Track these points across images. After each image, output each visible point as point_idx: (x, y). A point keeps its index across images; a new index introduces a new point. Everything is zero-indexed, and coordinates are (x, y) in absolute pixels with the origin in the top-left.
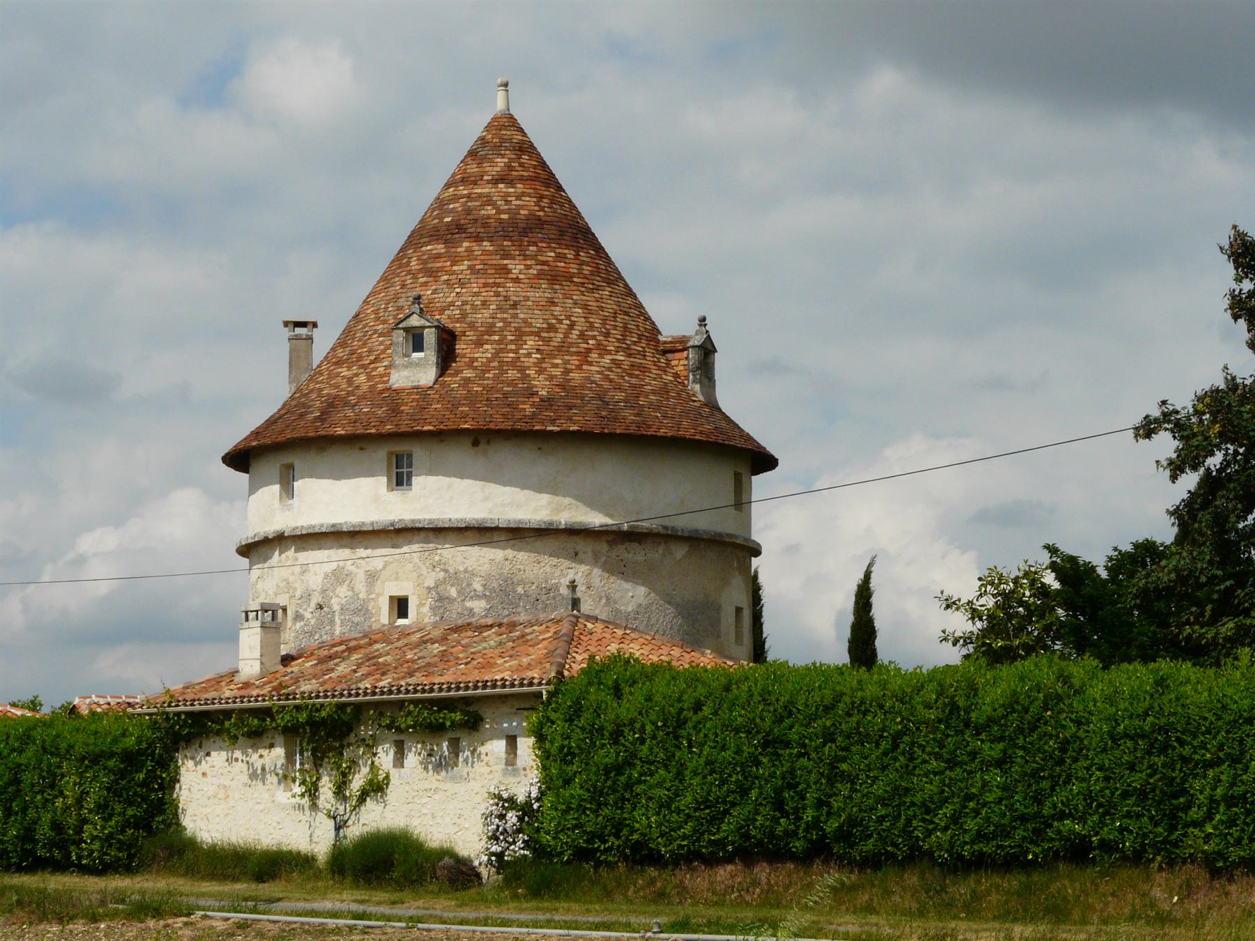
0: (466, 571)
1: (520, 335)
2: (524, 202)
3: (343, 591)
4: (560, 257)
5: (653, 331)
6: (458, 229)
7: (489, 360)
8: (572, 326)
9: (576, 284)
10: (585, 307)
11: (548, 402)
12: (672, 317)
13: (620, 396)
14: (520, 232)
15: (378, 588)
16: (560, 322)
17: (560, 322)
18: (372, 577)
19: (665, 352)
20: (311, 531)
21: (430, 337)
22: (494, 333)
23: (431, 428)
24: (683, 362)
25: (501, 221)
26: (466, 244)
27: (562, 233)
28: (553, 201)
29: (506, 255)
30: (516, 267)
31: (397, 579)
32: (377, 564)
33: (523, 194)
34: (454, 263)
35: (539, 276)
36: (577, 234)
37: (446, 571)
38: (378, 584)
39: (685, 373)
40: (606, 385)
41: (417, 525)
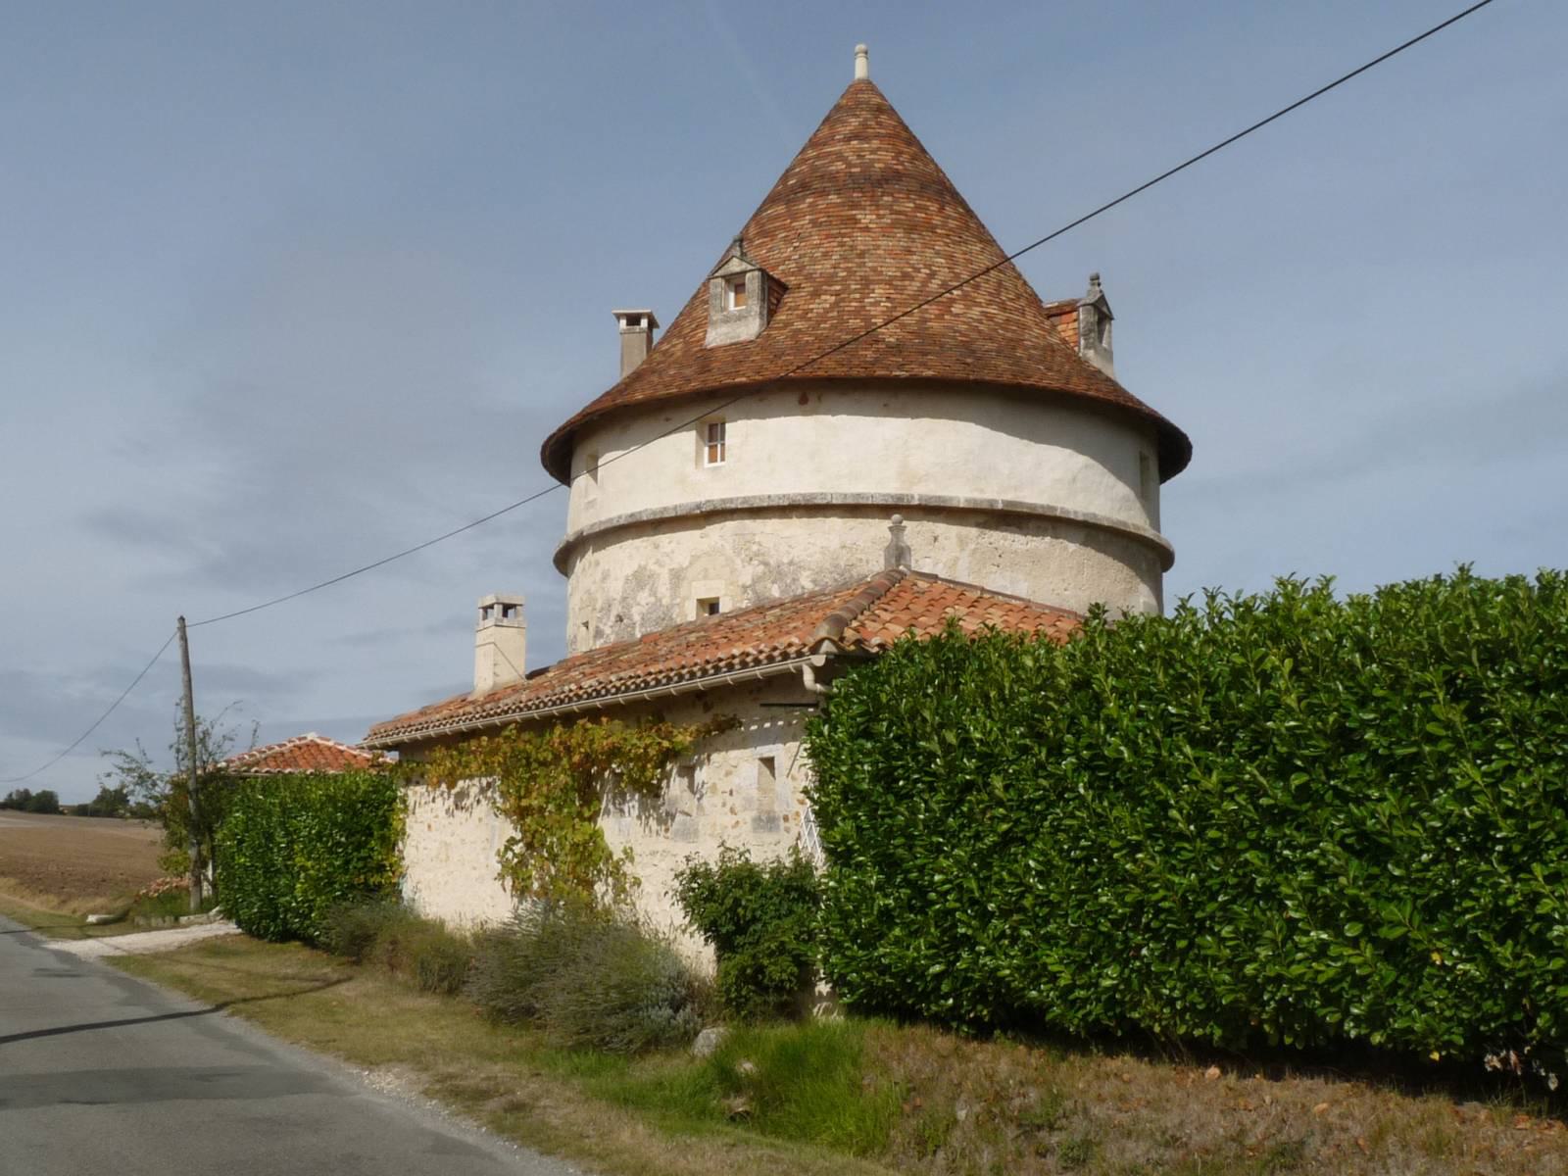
0: (791, 563)
1: (866, 284)
2: (881, 157)
3: (644, 597)
4: (918, 208)
5: (1034, 300)
6: (804, 186)
7: (827, 311)
8: (932, 275)
9: (940, 235)
10: (950, 257)
11: (898, 348)
12: (1053, 280)
13: (989, 345)
14: (874, 184)
15: (683, 591)
16: (918, 270)
17: (918, 270)
18: (677, 577)
19: (1049, 317)
20: (609, 525)
21: (753, 281)
22: (836, 283)
23: (744, 379)
24: (1071, 326)
25: (851, 175)
26: (809, 200)
27: (923, 187)
28: (914, 158)
29: (855, 206)
30: (866, 218)
31: (705, 577)
32: (681, 559)
33: (879, 149)
34: (795, 219)
35: (894, 225)
36: (943, 191)
37: (766, 564)
38: (685, 584)
39: (1074, 338)
40: (974, 335)
41: (729, 506)
